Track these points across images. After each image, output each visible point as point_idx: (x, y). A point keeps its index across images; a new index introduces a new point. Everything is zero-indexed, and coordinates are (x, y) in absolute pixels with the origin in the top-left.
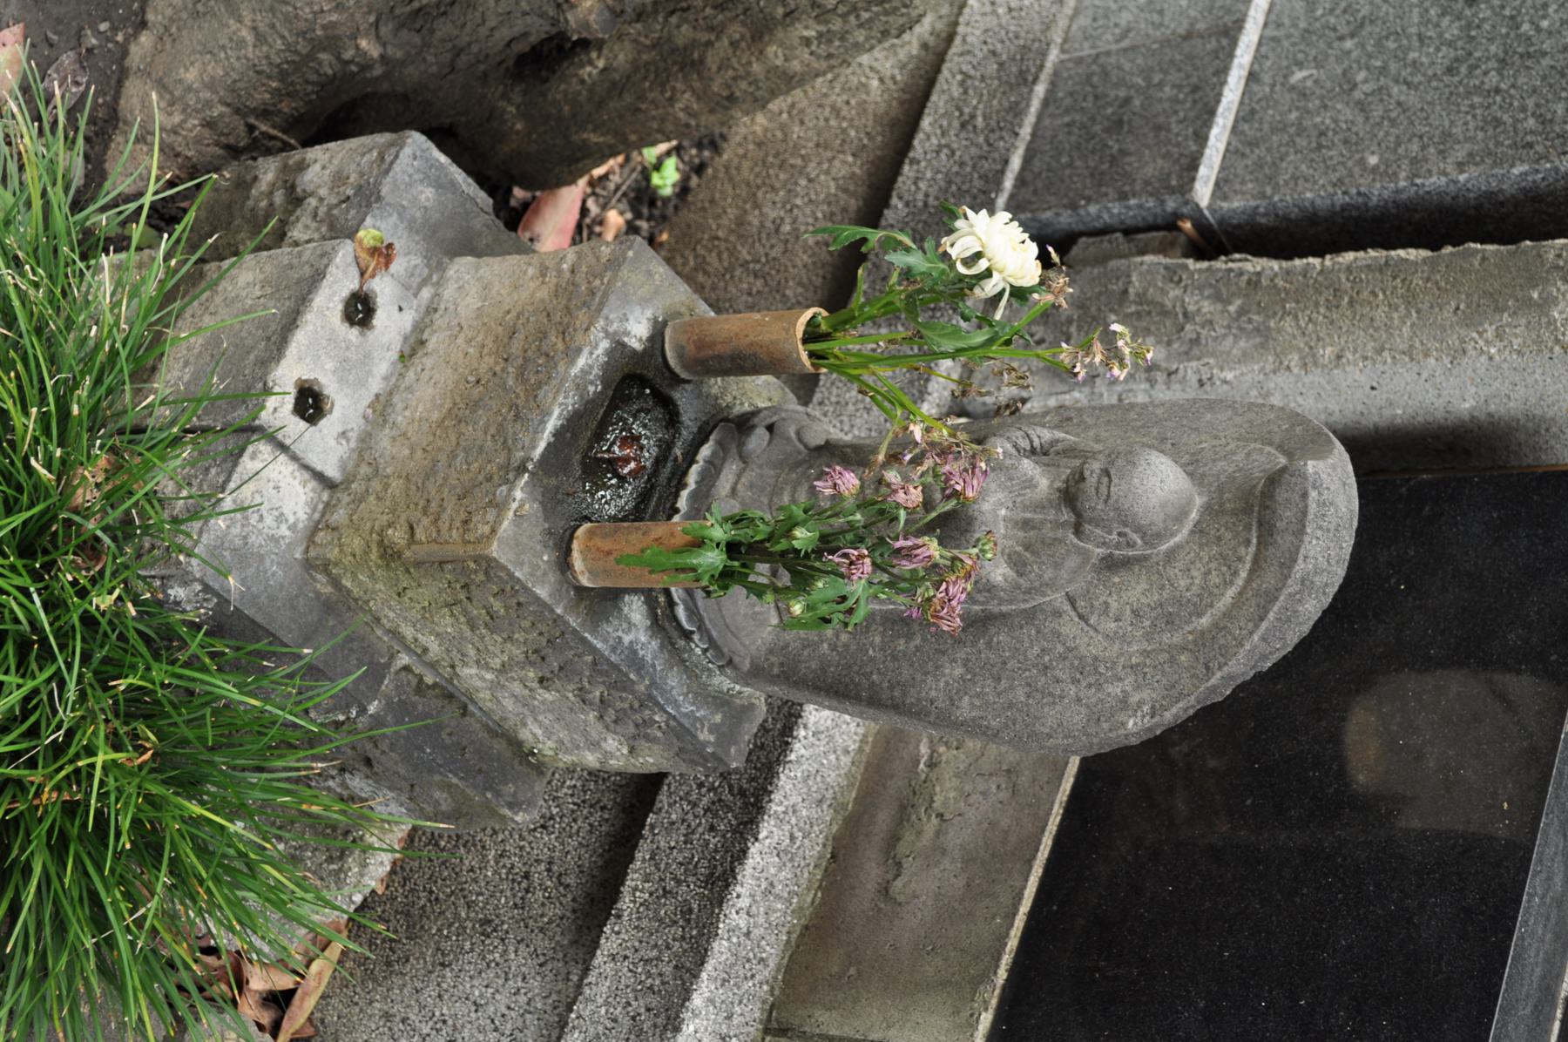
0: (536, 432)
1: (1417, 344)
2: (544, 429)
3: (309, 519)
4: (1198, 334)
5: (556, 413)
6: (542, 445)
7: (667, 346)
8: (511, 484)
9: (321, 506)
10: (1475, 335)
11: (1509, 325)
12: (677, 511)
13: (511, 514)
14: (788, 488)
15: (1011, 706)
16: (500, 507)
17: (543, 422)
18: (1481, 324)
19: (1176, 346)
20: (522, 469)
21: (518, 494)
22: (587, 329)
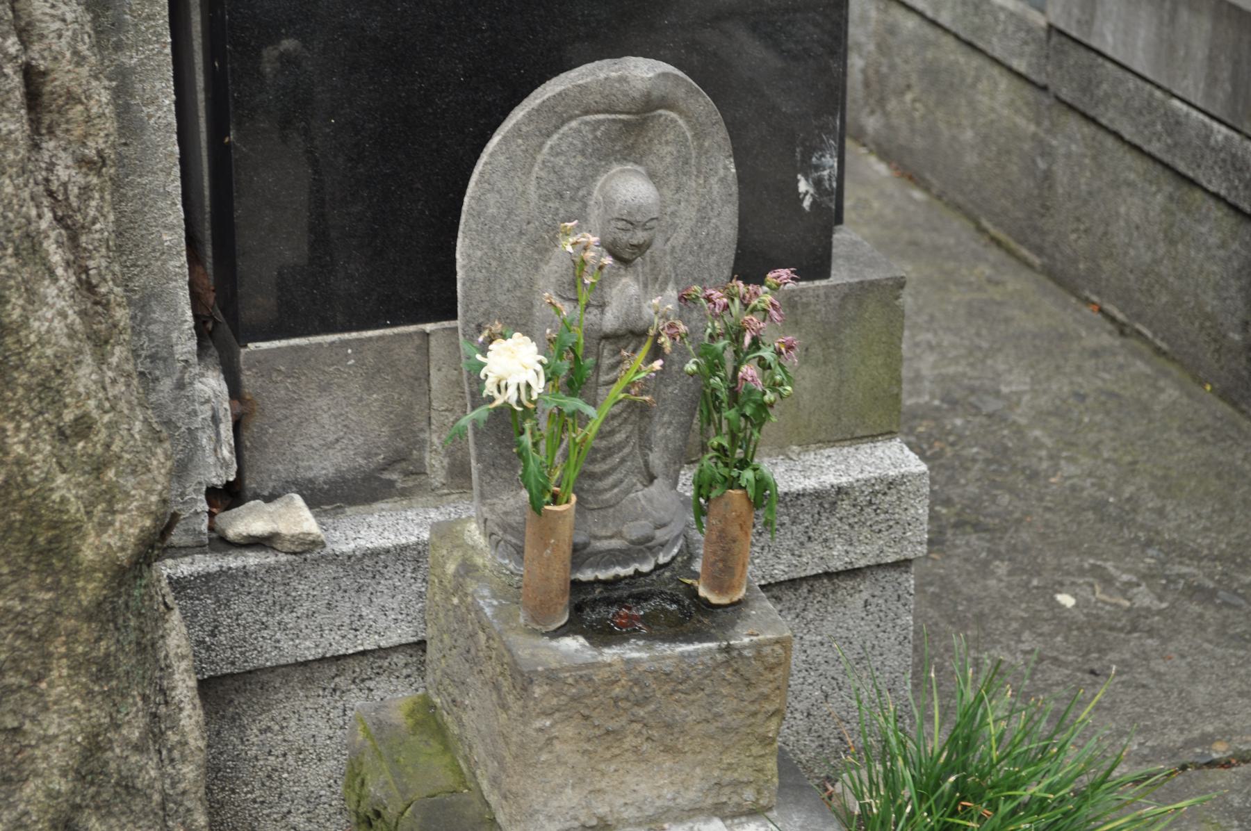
0: (698, 656)
1: (160, 166)
2: (696, 651)
3: (747, 822)
4: (146, 357)
5: (680, 649)
6: (706, 645)
7: (563, 622)
8: (740, 649)
9: (736, 821)
10: (152, 121)
11: (142, 97)
12: (636, 571)
13: (761, 637)
14: (600, 498)
15: (718, 265)
16: (758, 647)
17: (690, 655)
18: (141, 119)
19: (157, 373)
20: (728, 649)
21: (746, 640)
22: (610, 665)
